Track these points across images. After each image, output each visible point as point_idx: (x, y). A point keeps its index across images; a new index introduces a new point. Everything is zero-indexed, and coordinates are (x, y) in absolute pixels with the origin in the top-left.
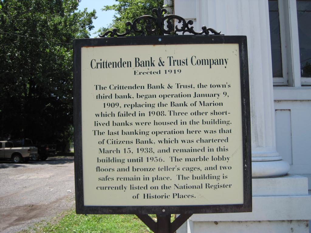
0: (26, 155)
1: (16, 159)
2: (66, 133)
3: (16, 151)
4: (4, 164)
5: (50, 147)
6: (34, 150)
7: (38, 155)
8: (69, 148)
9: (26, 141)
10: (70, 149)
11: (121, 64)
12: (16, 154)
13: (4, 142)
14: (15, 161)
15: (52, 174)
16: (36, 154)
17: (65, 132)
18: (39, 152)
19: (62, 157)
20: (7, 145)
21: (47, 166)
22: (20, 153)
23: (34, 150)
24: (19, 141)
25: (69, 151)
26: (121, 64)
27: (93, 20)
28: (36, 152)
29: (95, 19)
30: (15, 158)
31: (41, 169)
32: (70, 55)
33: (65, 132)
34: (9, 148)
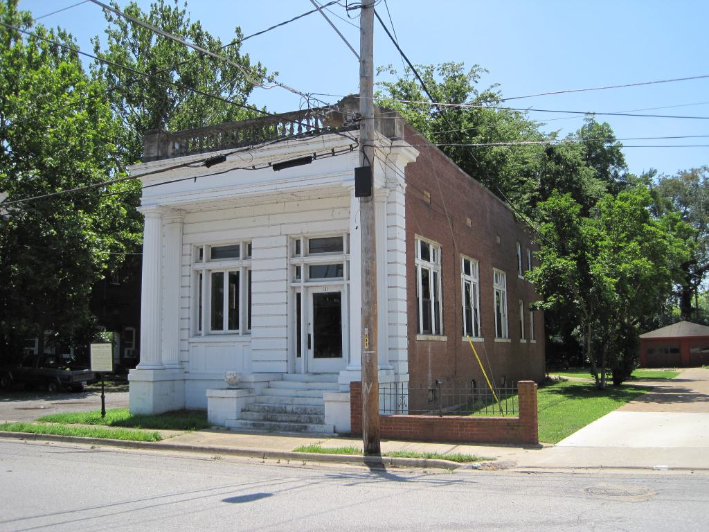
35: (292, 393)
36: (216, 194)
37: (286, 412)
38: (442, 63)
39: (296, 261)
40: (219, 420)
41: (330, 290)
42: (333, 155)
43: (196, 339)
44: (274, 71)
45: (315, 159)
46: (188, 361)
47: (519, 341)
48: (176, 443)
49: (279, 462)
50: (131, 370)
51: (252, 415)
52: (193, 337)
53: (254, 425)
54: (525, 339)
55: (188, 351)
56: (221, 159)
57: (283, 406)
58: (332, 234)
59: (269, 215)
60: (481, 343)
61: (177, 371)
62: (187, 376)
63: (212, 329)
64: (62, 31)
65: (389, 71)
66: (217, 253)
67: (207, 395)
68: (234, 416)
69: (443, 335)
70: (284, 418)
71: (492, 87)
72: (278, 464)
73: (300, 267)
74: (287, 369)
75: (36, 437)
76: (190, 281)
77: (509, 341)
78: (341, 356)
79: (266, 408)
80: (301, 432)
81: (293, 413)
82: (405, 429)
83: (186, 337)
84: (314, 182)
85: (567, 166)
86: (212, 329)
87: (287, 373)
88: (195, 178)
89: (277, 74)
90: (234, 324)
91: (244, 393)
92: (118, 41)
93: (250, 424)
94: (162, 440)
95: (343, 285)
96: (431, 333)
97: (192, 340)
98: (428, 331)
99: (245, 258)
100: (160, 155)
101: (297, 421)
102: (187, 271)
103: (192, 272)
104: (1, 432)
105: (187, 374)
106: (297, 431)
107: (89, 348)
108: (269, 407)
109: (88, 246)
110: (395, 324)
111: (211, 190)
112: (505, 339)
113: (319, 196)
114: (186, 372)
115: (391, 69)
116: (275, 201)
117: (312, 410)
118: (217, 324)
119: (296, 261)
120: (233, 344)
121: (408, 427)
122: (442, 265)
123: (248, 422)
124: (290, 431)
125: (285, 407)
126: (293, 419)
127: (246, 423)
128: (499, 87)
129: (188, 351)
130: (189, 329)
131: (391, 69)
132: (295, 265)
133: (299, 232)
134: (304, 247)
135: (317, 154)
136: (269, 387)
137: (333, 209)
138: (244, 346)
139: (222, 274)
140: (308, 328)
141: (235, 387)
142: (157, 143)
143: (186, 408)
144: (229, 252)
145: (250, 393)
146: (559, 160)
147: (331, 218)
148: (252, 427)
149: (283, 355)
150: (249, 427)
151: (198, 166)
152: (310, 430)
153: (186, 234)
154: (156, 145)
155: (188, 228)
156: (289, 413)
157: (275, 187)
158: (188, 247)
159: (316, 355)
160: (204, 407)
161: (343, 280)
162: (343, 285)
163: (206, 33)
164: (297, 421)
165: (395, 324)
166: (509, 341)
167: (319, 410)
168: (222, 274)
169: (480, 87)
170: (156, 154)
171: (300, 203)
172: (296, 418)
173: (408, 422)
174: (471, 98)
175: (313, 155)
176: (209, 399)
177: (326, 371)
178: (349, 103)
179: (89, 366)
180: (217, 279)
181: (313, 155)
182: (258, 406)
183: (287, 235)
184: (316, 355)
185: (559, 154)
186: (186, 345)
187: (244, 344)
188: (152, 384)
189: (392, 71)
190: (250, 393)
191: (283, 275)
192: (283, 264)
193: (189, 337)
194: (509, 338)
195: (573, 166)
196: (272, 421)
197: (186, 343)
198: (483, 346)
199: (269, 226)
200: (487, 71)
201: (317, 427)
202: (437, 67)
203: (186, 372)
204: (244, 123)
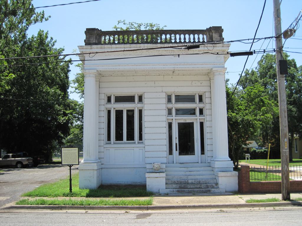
0: (24, 163)
1: (19, 165)
2: (49, 146)
3: (19, 161)
4: (12, 169)
5: (41, 158)
6: (30, 160)
7: (33, 163)
8: (52, 158)
9: (24, 154)
10: (53, 159)
11: (66, 150)
12: (19, 162)
13: (186, 190)
14: (18, 167)
15: (46, 173)
16: (31, 162)
17: (49, 145)
18: (33, 161)
19: (47, 165)
20: (13, 157)
21: (37, 169)
22: (21, 161)
23: (30, 160)
24: (19, 154)
25: (52, 160)
26: (66, 150)
27: (70, 65)
28: (32, 161)
29: (71, 64)
30: (18, 165)
31: (39, 171)
32: (53, 91)
33: (49, 145)
34: (14, 159)
35: (183, 173)
36: (136, 67)
37: (188, 183)
38: (146, 23)
39: (170, 106)
40: (155, 190)
41: (188, 121)
43: (108, 146)
44: (49, 16)
45: (255, 53)
49: (274, 209)
51: (172, 186)
53: (178, 191)
57: (187, 180)
58: (190, 94)
62: (103, 166)
63: (116, 141)
65: (123, 23)
66: (120, 99)
68: (164, 186)
70: (192, 187)
72: (259, 210)
75: (61, 208)
76: (105, 114)
78: (194, 154)
79: (176, 182)
80: (207, 193)
81: (192, 183)
82: (271, 188)
84: (197, 66)
86: (116, 141)
88: (179, 55)
89: (50, 17)
90: (130, 137)
93: (176, 191)
95: (197, 119)
97: (106, 146)
101: (200, 188)
102: (103, 108)
105: (102, 165)
106: (205, 192)
108: (177, 181)
111: (133, 65)
113: (183, 74)
114: (102, 164)
116: (159, 74)
117: (203, 182)
118: (119, 137)
119: (170, 106)
120: (133, 148)
121: (273, 187)
123: (174, 190)
124: (202, 193)
125: (188, 181)
126: (197, 187)
127: (173, 191)
133: (173, 91)
134: (113, 99)
135: (256, 51)
137: (192, 81)
138: (115, 150)
139: (122, 111)
140: (175, 140)
142: (95, 35)
143: (103, 184)
144: (130, 99)
147: (191, 85)
148: (177, 192)
150: (175, 192)
151: (181, 49)
152: (212, 192)
154: (95, 37)
156: (190, 184)
157: (173, 66)
159: (180, 154)
160: (143, 183)
161: (173, 117)
162: (197, 119)
164: (200, 188)
167: (207, 181)
168: (122, 111)
171: (173, 76)
172: (199, 186)
173: (273, 184)
175: (253, 51)
176: (147, 179)
177: (186, 162)
178: (215, 30)
180: (119, 113)
181: (253, 51)
182: (171, 181)
183: (165, 92)
184: (180, 154)
186: (102, 149)
187: (140, 148)
192: (164, 107)
196: (185, 188)
199: (155, 87)
201: (216, 190)
202: (144, 25)
203: (102, 164)
204: (153, 32)
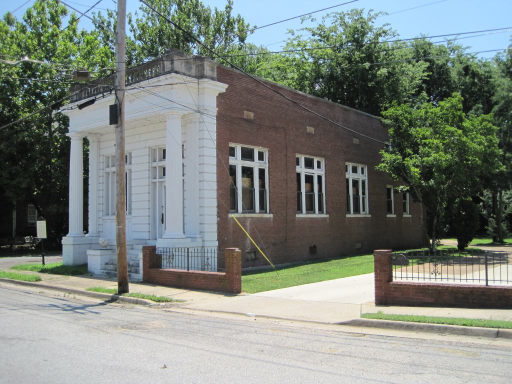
39: (154, 164)
42: (104, 97)
46: (102, 232)
47: (386, 216)
48: (54, 285)
50: (63, 237)
52: (105, 216)
54: (395, 214)
55: (102, 225)
56: (92, 102)
59: (140, 134)
60: (410, 217)
61: (94, 238)
64: (110, 12)
65: (310, 20)
67: (88, 253)
68: (99, 267)
69: (270, 213)
71: (384, 25)
73: (318, 168)
74: (149, 236)
77: (370, 216)
83: (101, 216)
85: (480, 79)
87: (149, 239)
91: (109, 252)
92: (148, 14)
94: (41, 280)
96: (323, 213)
97: (104, 218)
98: (322, 212)
99: (160, 160)
100: (78, 98)
103: (104, 173)
104: (1, 278)
107: (35, 224)
109: (486, 147)
110: (203, 207)
112: (364, 214)
115: (312, 18)
119: (154, 164)
122: (269, 163)
128: (389, 26)
129: (102, 225)
130: (103, 211)
131: (312, 18)
132: (162, 167)
133: (154, 145)
136: (132, 249)
141: (105, 248)
145: (113, 252)
146: (474, 75)
149: (146, 228)
153: (102, 149)
155: (102, 145)
158: (102, 157)
163: (201, 3)
165: (203, 207)
166: (370, 216)
169: (377, 25)
170: (75, 99)
174: (370, 36)
179: (36, 236)
185: (473, 70)
188: (72, 246)
189: (313, 19)
190: (113, 252)
191: (146, 174)
192: (146, 167)
193: (103, 216)
194: (369, 214)
195: (485, 78)
197: (101, 219)
198: (328, 221)
200: (387, 14)
